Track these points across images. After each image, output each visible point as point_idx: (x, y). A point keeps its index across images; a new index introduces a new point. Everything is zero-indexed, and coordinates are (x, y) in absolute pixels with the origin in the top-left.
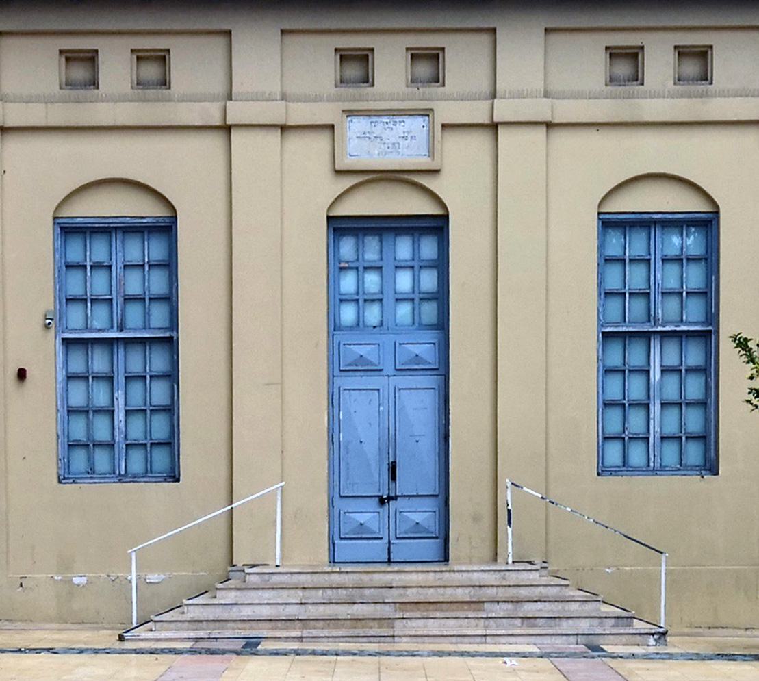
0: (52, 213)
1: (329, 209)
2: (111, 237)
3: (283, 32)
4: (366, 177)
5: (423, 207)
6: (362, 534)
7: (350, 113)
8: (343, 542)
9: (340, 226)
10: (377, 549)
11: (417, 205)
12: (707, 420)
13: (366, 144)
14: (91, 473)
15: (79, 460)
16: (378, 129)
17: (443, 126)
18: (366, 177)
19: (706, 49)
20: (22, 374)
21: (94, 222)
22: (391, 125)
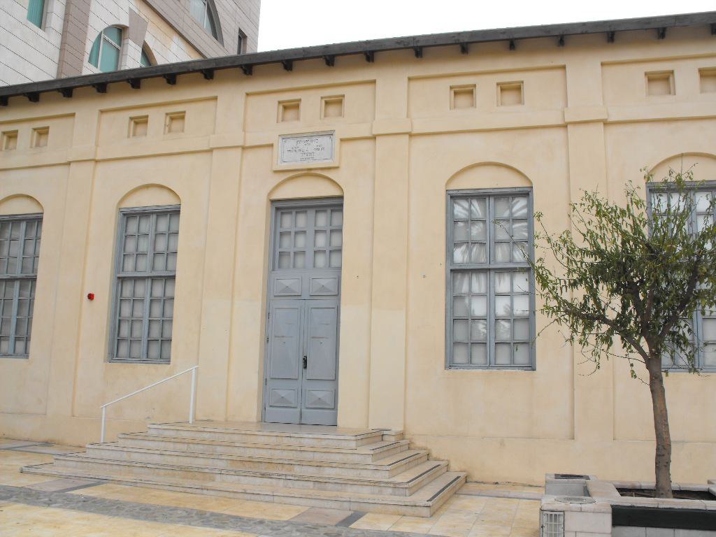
0: (444, 187)
1: (447, 184)
2: (485, 202)
3: (602, 64)
4: (291, 174)
5: (330, 191)
6: (284, 404)
7: (285, 137)
8: (271, 409)
9: (281, 207)
10: (292, 415)
11: (510, 182)
12: (453, 308)
13: (288, 157)
14: (470, 364)
15: (460, 355)
16: (301, 146)
17: (342, 140)
18: (291, 174)
19: (667, 74)
20: (91, 297)
21: (324, 201)
22: (309, 142)
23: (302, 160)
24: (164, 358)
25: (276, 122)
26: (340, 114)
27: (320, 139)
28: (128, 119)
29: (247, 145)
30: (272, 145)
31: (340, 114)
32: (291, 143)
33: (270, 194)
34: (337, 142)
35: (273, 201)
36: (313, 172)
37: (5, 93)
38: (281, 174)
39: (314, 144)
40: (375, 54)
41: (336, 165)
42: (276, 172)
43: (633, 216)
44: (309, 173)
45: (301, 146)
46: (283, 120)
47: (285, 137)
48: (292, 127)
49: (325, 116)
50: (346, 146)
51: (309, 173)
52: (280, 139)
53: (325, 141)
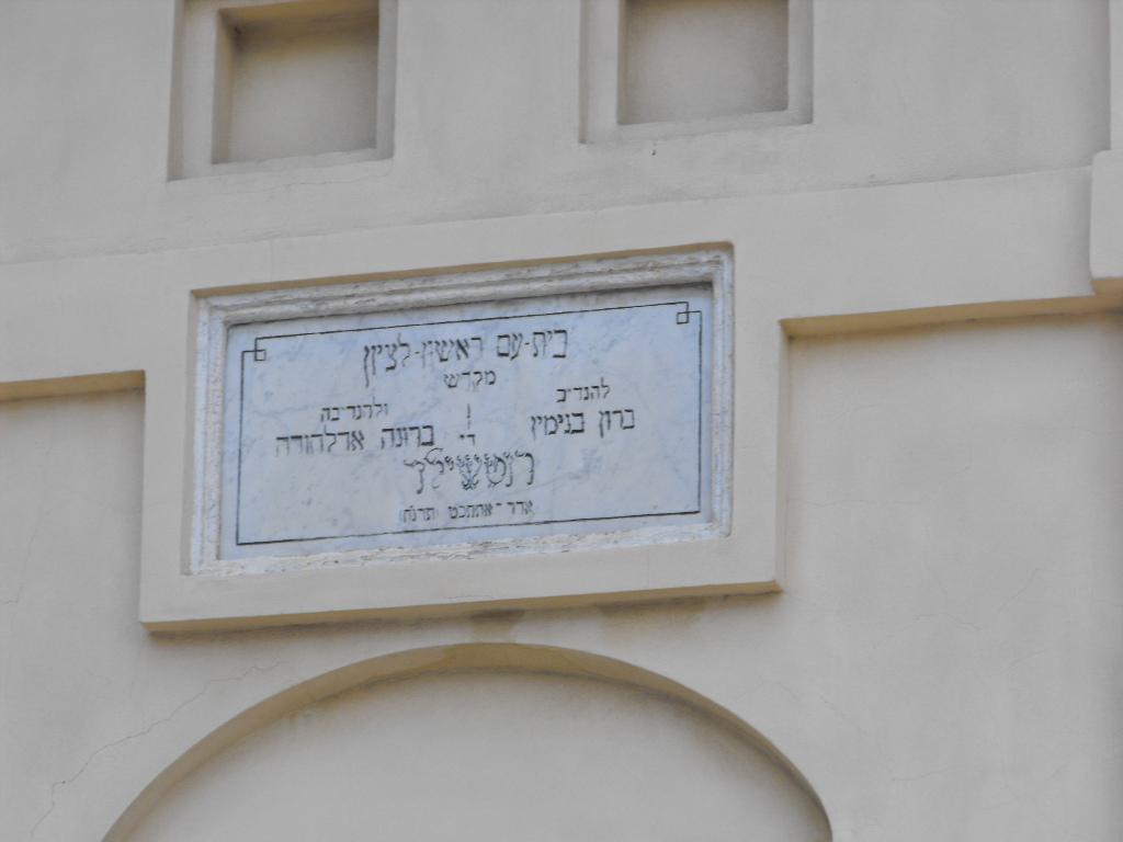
7: (251, 313)
16: (411, 391)
17: (799, 336)
22: (485, 359)
24: (784, 324)
25: (161, 167)
26: (774, 95)
28: (185, 300)
30: (130, 388)
31: (774, 95)
32: (309, 370)
34: (758, 349)
36: (524, 636)
37: (793, 4)
38: (225, 662)
39: (535, 379)
41: (751, 571)
42: (170, 636)
43: (470, 553)
45: (411, 391)
46: (221, 156)
47: (251, 313)
48: (321, 211)
49: (629, 113)
50: (843, 390)
53: (635, 346)
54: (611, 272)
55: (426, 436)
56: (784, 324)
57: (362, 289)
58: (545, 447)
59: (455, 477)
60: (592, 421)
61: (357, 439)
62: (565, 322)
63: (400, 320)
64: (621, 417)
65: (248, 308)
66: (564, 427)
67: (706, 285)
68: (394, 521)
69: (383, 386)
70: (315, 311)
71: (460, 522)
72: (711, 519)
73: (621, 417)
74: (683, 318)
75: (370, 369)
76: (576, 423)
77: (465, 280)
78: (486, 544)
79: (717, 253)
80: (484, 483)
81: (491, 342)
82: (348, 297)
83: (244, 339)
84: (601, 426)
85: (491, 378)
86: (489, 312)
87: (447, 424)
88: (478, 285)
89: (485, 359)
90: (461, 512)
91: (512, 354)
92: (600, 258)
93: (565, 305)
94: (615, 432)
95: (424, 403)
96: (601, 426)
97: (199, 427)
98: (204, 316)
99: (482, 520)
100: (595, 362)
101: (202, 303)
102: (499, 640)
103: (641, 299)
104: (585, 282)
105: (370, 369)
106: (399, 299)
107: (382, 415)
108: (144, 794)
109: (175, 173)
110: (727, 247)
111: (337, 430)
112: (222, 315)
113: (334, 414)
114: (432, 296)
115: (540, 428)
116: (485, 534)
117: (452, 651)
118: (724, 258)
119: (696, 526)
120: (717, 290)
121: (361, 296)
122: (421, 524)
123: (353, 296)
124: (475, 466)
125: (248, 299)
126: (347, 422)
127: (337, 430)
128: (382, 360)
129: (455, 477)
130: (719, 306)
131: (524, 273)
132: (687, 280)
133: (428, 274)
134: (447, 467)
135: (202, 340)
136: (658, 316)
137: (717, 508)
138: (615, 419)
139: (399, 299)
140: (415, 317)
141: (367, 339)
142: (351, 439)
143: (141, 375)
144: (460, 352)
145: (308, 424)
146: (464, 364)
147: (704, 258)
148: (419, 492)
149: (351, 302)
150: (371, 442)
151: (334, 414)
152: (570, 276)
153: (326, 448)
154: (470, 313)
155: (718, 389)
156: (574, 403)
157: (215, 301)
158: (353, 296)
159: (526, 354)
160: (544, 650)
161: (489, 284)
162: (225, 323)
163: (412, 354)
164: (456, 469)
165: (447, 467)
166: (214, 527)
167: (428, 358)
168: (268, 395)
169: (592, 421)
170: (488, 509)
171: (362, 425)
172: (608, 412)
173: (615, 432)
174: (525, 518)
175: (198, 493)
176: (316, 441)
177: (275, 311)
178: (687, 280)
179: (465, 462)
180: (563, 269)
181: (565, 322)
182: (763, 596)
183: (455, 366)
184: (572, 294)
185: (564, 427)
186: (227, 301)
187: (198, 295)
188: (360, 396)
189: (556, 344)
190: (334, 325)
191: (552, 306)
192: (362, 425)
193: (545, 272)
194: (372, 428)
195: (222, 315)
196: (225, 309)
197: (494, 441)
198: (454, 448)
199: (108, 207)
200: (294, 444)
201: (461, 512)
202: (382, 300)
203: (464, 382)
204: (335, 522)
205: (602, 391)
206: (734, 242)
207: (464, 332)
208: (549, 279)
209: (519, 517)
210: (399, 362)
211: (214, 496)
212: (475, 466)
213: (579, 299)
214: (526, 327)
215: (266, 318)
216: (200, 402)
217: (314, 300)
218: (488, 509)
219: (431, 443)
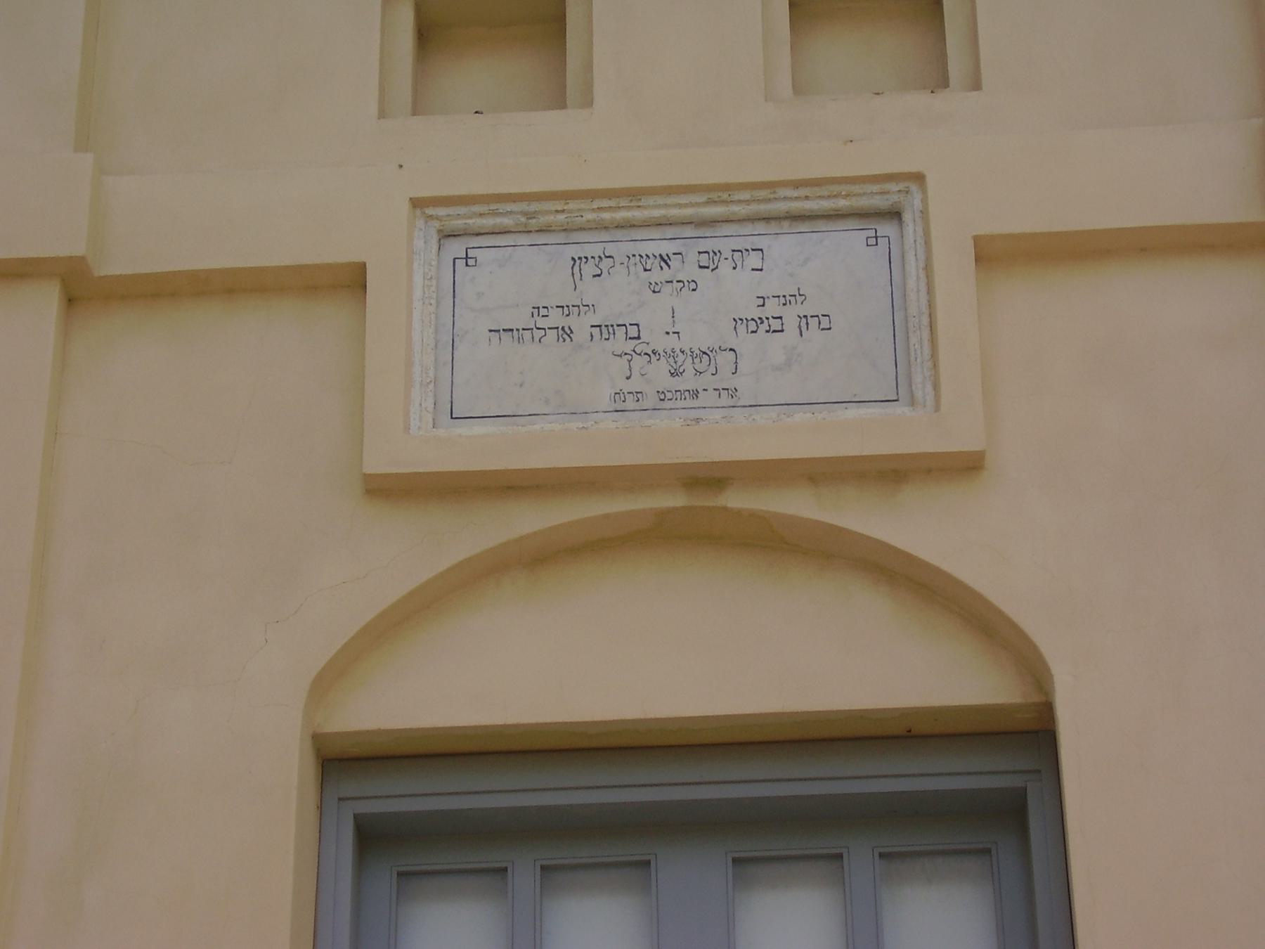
7: (462, 223)
13: (496, 368)
16: (617, 294)
17: (992, 255)
22: (679, 270)
23: (621, 403)
24: (977, 240)
25: (374, 109)
27: (783, 247)
29: (116, 264)
30: (353, 281)
32: (515, 276)
33: (328, 681)
35: (338, 762)
36: (735, 500)
39: (736, 288)
40: (896, 222)
42: (391, 490)
44: (704, 517)
45: (617, 294)
47: (462, 223)
51: (704, 517)
52: (425, 240)
53: (832, 264)
54: (807, 198)
55: (633, 332)
56: (977, 240)
57: (572, 205)
58: (746, 343)
59: (663, 366)
60: (791, 323)
61: (566, 333)
62: (761, 242)
63: (605, 236)
64: (823, 321)
65: (458, 218)
66: (765, 327)
67: (895, 215)
68: (606, 403)
69: (590, 290)
70: (526, 225)
71: (668, 404)
72: (912, 402)
73: (823, 321)
74: (872, 241)
75: (577, 276)
76: (776, 325)
77: (670, 200)
78: (697, 420)
79: (906, 184)
80: (690, 372)
81: (692, 257)
82: (557, 211)
83: (456, 248)
84: (800, 327)
85: (693, 286)
86: (689, 231)
87: (653, 318)
88: (680, 206)
89: (689, 271)
90: (669, 395)
91: (712, 267)
92: (797, 184)
93: (760, 228)
94: (813, 332)
95: (629, 305)
96: (800, 327)
97: (416, 315)
98: (420, 223)
99: (690, 403)
100: (791, 275)
101: (418, 212)
102: (706, 504)
103: (831, 226)
104: (782, 207)
105: (577, 276)
106: (606, 216)
107: (590, 314)
108: (345, 647)
109: (382, 114)
110: (919, 178)
111: (550, 325)
112: (437, 224)
113: (544, 312)
114: (637, 214)
115: (742, 328)
116: (694, 414)
117: (663, 515)
118: (914, 188)
119: (900, 410)
120: (907, 217)
121: (571, 211)
122: (630, 404)
123: (563, 211)
124: (681, 358)
125: (462, 210)
126: (556, 318)
127: (550, 325)
128: (589, 269)
129: (663, 366)
130: (909, 229)
131: (725, 196)
132: (879, 210)
133: (634, 194)
134: (654, 358)
135: (419, 244)
136: (848, 242)
137: (919, 394)
138: (813, 322)
139: (606, 216)
140: (619, 234)
141: (575, 251)
142: (561, 332)
143: (363, 267)
144: (663, 264)
145: (520, 319)
146: (667, 274)
147: (893, 187)
148: (628, 378)
149: (561, 217)
150: (581, 334)
151: (544, 312)
152: (768, 201)
153: (537, 339)
154: (670, 232)
155: (912, 296)
156: (772, 308)
157: (430, 211)
158: (563, 211)
159: (725, 268)
160: (754, 516)
161: (692, 205)
162: (440, 231)
163: (617, 264)
164: (663, 360)
165: (654, 358)
166: (430, 401)
167: (632, 268)
168: (480, 295)
169: (791, 323)
170: (695, 394)
171: (572, 322)
172: (805, 316)
173: (813, 332)
174: (731, 402)
175: (417, 370)
176: (527, 334)
177: (489, 222)
178: (879, 210)
179: (671, 354)
180: (762, 194)
181: (761, 242)
182: (966, 466)
183: (657, 276)
184: (767, 219)
185: (765, 327)
186: (441, 212)
187: (417, 203)
188: (570, 298)
189: (754, 260)
190: (541, 239)
191: (748, 229)
192: (572, 322)
193: (745, 195)
194: (581, 325)
195: (437, 224)
196: (438, 218)
197: (698, 336)
198: (661, 343)
199: (325, 141)
200: (504, 336)
201: (669, 395)
202: (590, 216)
203: (667, 289)
204: (547, 402)
205: (800, 299)
206: (926, 173)
207: (666, 248)
208: (747, 202)
209: (725, 400)
210: (605, 271)
211: (431, 374)
212: (681, 358)
213: (773, 223)
214: (725, 246)
215: (478, 230)
216: (418, 293)
217: (524, 214)
218: (695, 394)
219: (639, 338)
